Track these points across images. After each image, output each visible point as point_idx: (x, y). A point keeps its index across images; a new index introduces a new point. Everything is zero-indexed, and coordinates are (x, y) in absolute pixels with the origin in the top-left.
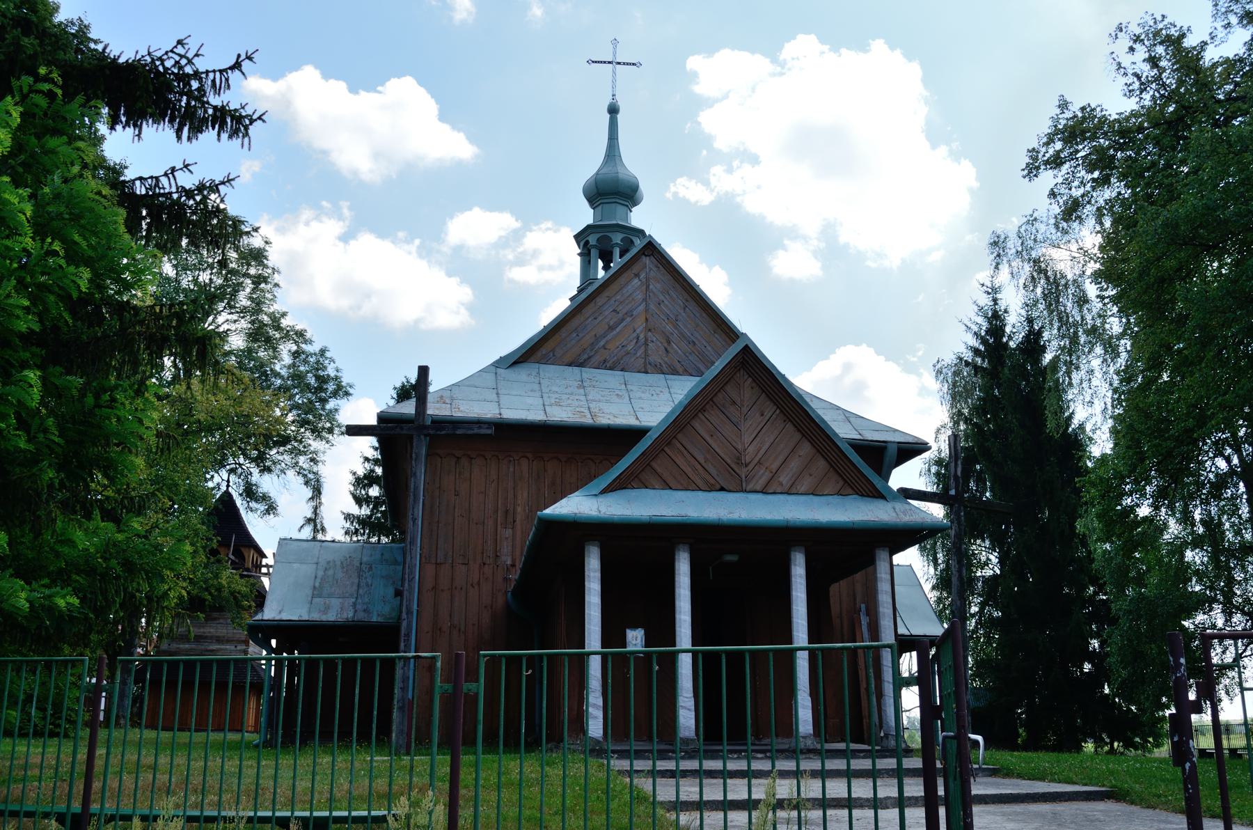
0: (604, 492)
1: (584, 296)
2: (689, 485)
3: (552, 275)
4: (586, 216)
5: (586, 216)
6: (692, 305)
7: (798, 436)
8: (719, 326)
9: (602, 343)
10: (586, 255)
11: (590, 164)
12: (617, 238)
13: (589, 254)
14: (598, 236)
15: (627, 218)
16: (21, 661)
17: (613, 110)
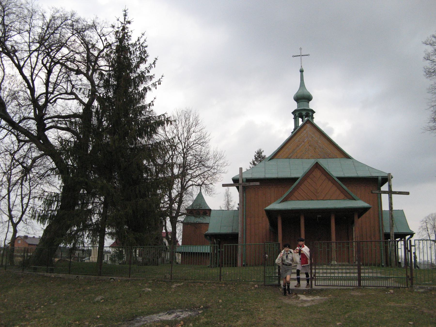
0: (281, 202)
2: (303, 199)
3: (282, 128)
4: (294, 106)
5: (294, 106)
6: (322, 138)
7: (332, 184)
11: (295, 89)
15: (308, 106)
17: (302, 71)
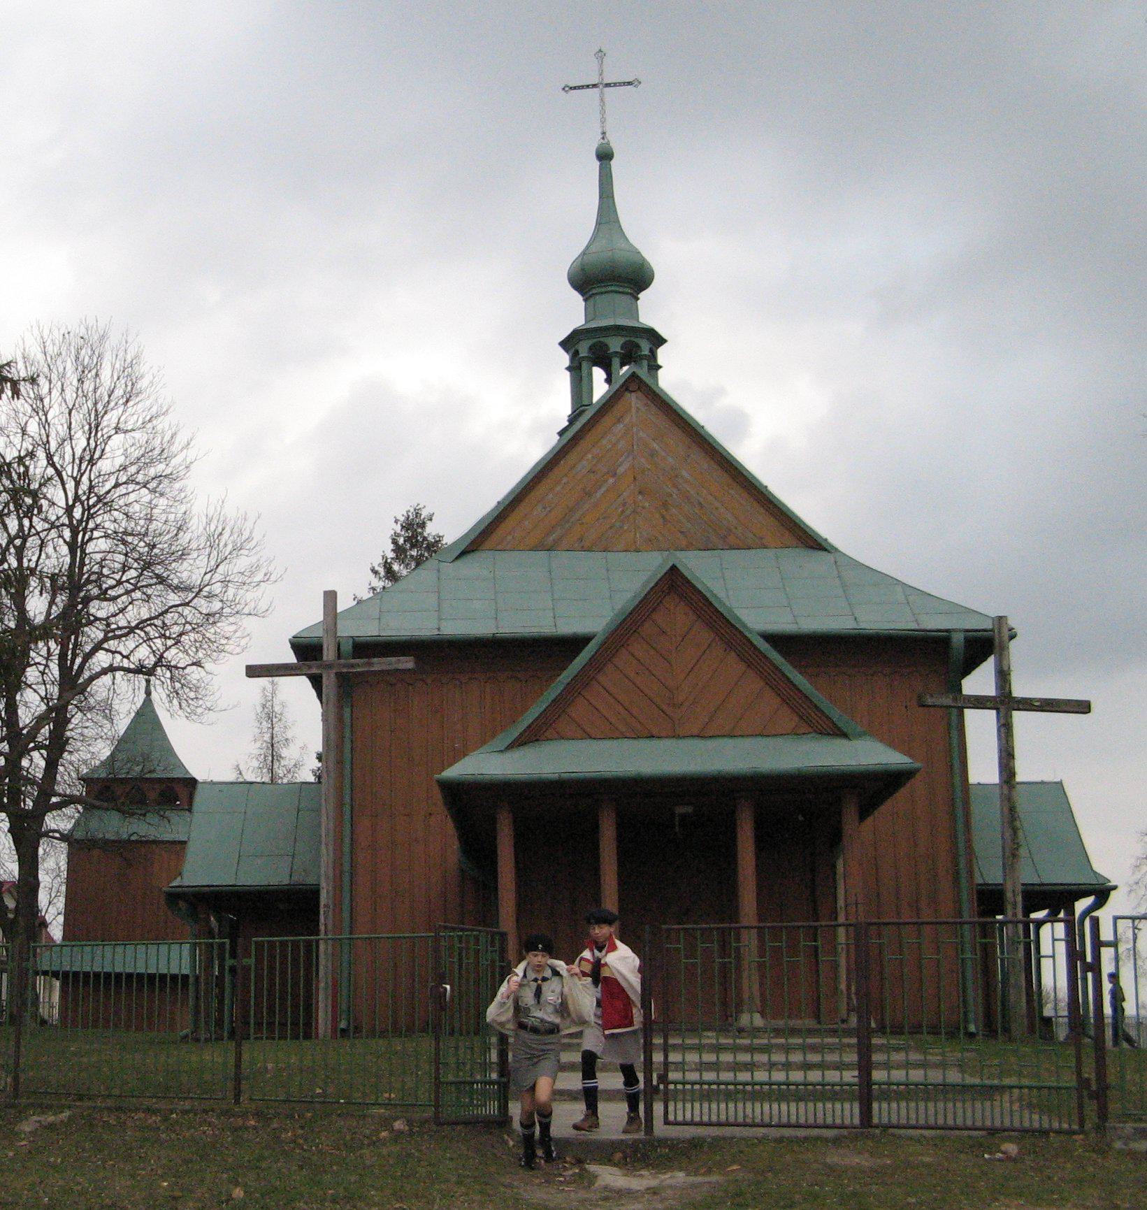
0: (511, 747)
1: (578, 425)
4: (572, 312)
5: (572, 312)
6: (697, 455)
8: (734, 478)
9: (577, 515)
10: (577, 370)
11: (574, 236)
12: (615, 344)
13: (579, 367)
14: (590, 342)
15: (635, 313)
16: (679, 930)
